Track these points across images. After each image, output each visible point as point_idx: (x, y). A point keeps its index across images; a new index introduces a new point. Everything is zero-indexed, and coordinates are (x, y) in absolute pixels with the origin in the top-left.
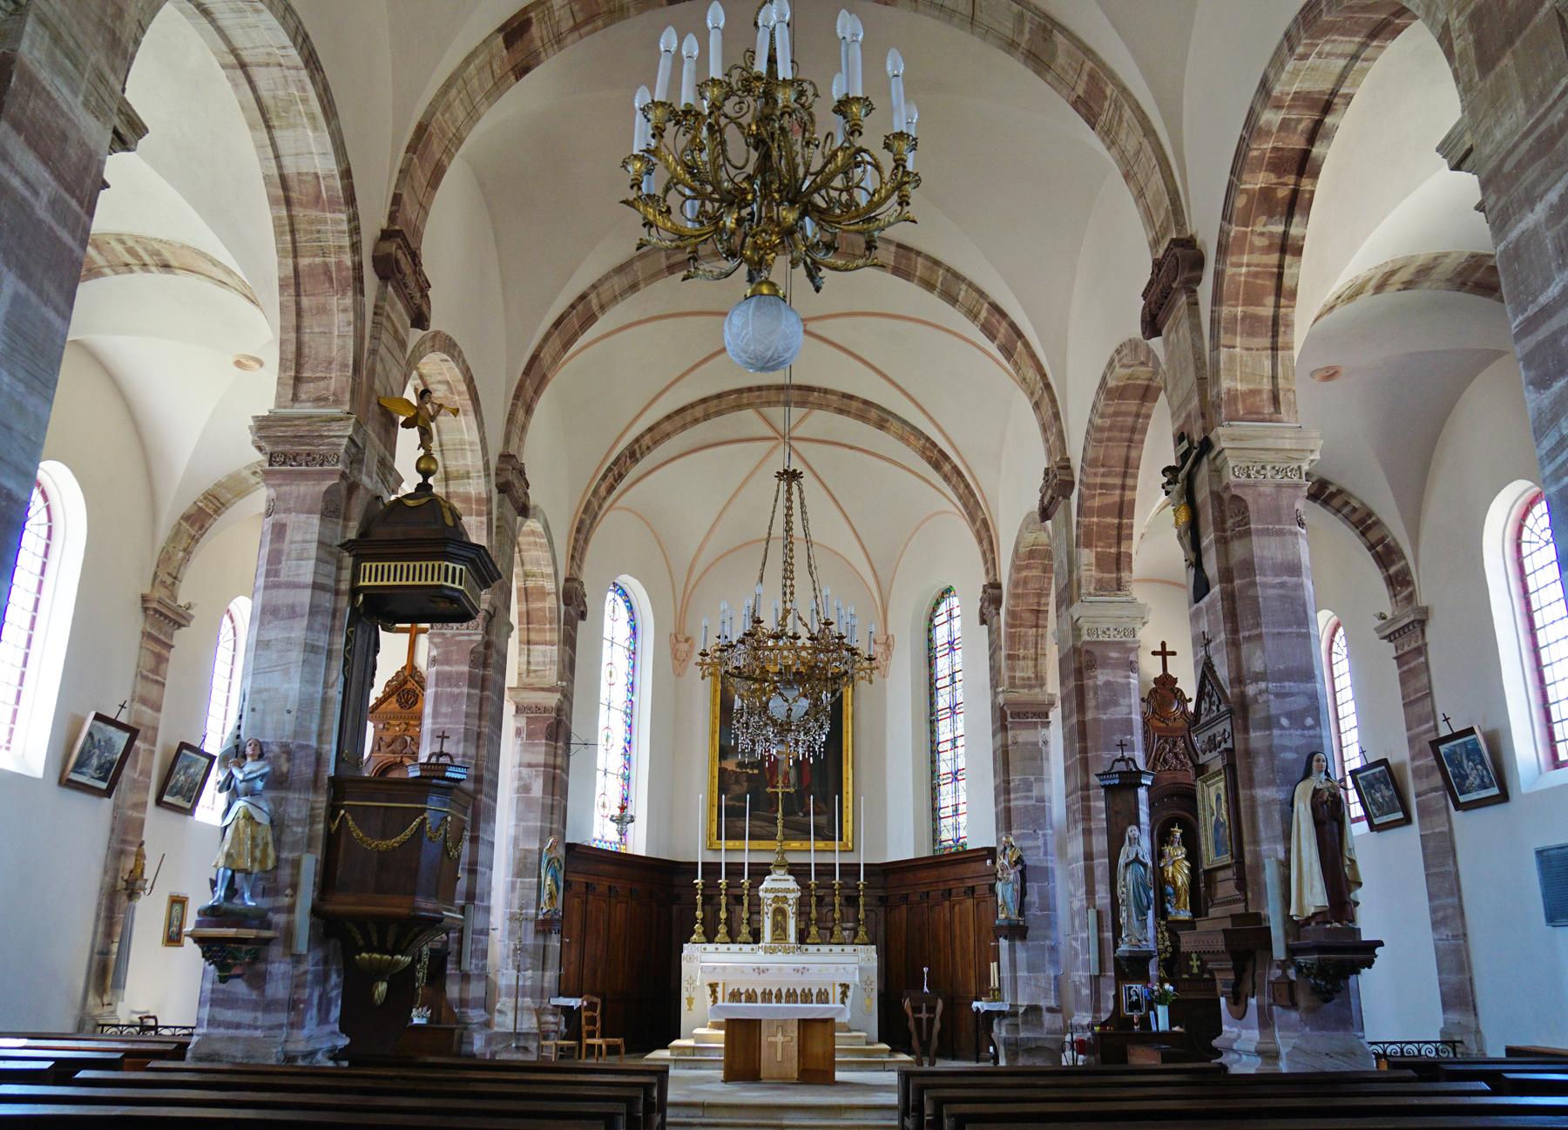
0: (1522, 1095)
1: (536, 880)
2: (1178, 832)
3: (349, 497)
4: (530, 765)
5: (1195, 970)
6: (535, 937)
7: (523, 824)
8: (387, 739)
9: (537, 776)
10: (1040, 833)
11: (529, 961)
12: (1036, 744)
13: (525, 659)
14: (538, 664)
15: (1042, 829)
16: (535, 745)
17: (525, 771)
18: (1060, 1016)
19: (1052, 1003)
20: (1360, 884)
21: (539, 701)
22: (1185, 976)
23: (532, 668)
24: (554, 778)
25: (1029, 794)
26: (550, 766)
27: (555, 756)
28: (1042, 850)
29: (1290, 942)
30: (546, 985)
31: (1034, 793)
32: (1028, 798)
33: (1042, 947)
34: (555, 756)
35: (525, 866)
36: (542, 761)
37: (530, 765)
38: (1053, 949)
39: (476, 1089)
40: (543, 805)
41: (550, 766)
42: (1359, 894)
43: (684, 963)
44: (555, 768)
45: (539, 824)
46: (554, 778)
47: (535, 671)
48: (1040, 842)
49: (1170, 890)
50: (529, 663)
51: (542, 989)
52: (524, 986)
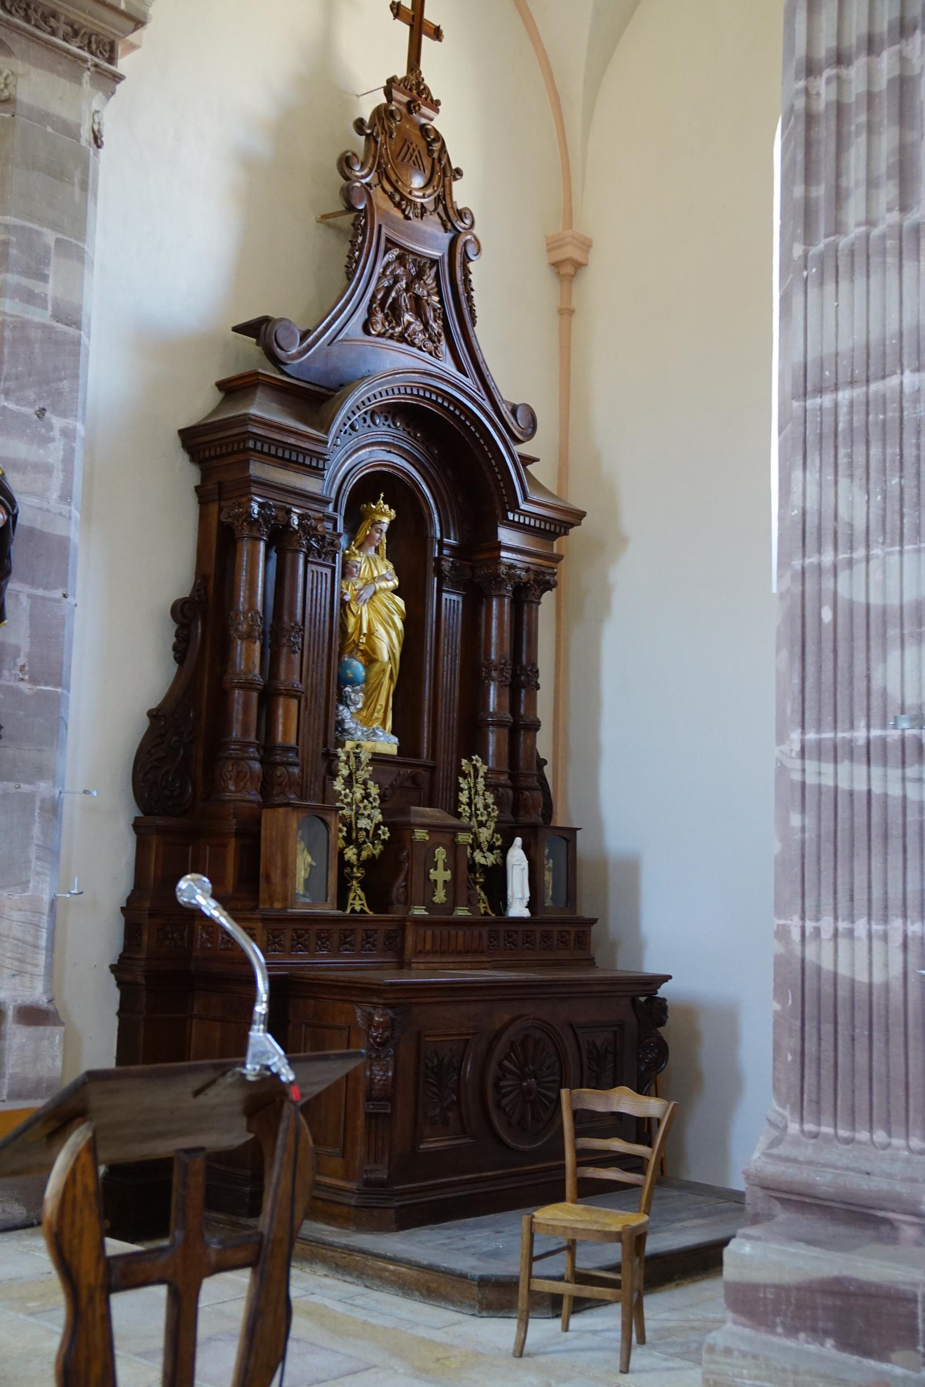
0: (771, 550)
2: (386, 516)
5: (440, 896)
10: (57, 422)
12: (72, 131)
15: (63, 414)
18: (55, 1034)
19: (36, 994)
20: (471, 273)
22: (419, 911)
25: (37, 287)
28: (57, 480)
31: (51, 289)
32: (30, 297)
33: (26, 801)
38: (53, 809)
39: (322, 1180)
42: (477, 319)
48: (54, 454)
49: (357, 667)
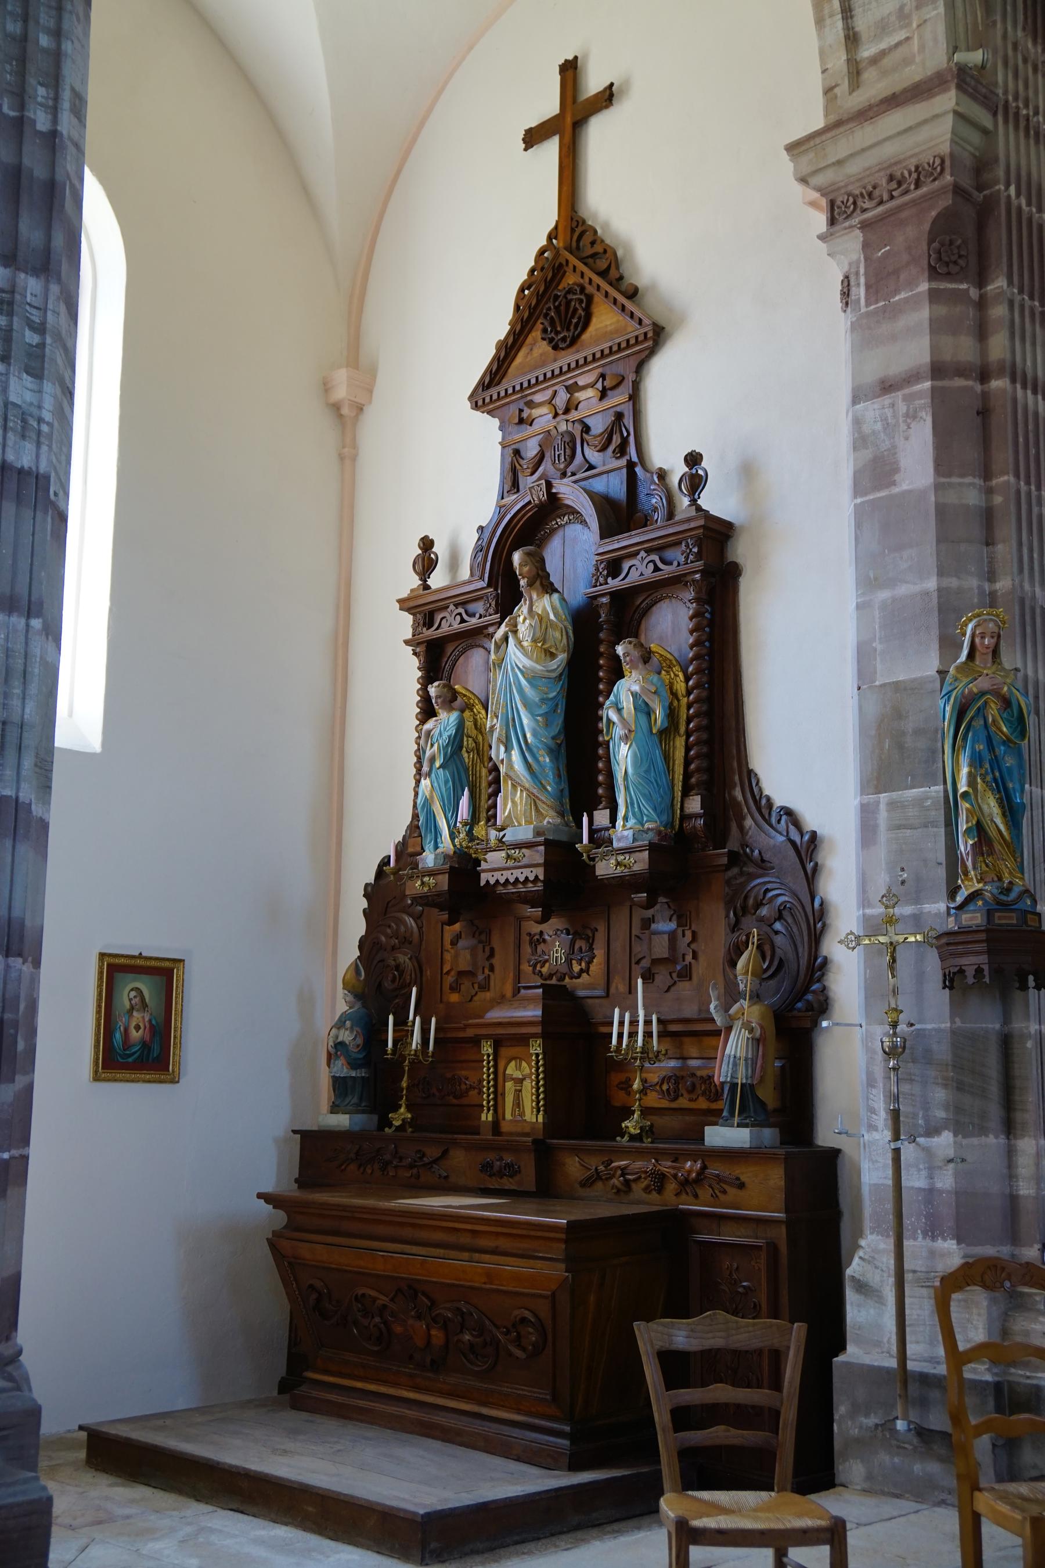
1: (941, 787)
3: (981, 227)
4: (887, 387)
6: (957, 1007)
7: (883, 595)
8: (531, 450)
9: (912, 416)
11: (940, 1095)
13: (836, 26)
14: (883, 28)
16: (892, 312)
17: (872, 410)
21: (889, 151)
23: (867, 52)
24: (984, 413)
26: (961, 371)
27: (982, 333)
29: (27, 968)
30: (1025, 1189)
34: (982, 333)
35: (900, 746)
36: (925, 358)
37: (887, 387)
40: (941, 511)
41: (961, 371)
43: (958, 1532)
44: (984, 376)
45: (931, 584)
46: (984, 413)
47: (875, 60)
50: (852, 39)
51: (1013, 1201)
52: (930, 1192)
